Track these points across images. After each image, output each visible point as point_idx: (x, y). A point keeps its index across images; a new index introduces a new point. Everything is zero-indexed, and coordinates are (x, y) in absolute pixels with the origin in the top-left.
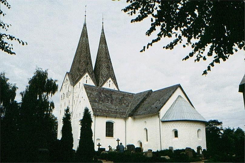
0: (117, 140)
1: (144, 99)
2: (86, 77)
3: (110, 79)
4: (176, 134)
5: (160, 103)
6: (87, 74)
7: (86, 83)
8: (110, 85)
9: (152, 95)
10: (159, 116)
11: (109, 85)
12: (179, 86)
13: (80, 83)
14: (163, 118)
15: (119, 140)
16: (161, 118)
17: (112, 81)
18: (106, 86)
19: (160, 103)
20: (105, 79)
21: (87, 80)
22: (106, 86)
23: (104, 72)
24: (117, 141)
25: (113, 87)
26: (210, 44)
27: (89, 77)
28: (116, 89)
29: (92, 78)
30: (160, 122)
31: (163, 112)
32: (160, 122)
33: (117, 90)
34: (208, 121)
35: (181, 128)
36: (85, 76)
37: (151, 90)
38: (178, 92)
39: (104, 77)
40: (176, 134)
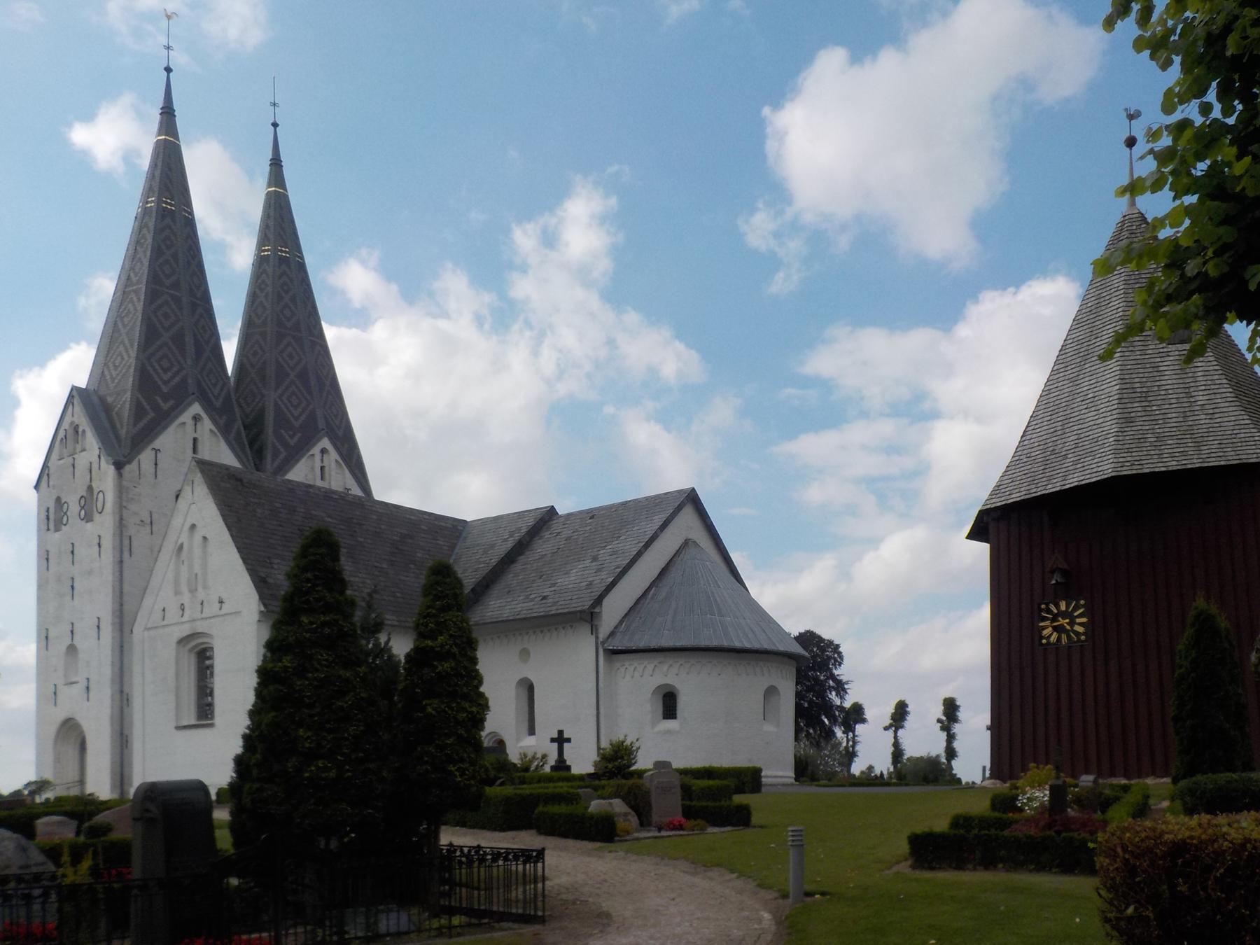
0: (553, 740)
1: (521, 548)
2: (190, 422)
3: (325, 443)
4: (669, 704)
5: (599, 570)
6: (196, 408)
7: (322, 478)
8: (322, 468)
9: (556, 526)
10: (594, 630)
11: (312, 469)
12: (691, 499)
13: (157, 451)
14: (612, 634)
15: (569, 740)
16: (604, 631)
17: (333, 455)
18: (299, 473)
19: (599, 570)
20: (296, 439)
21: (195, 440)
22: (299, 473)
23: (165, 363)
24: (555, 745)
25: (339, 480)
26: (959, 651)
27: (207, 424)
28: (356, 491)
29: (225, 431)
30: (597, 661)
31: (614, 609)
32: (597, 661)
33: (356, 491)
34: (482, 689)
35: (690, 681)
36: (186, 417)
37: (74, 389)
38: (687, 524)
39: (166, 398)
40: (669, 704)
